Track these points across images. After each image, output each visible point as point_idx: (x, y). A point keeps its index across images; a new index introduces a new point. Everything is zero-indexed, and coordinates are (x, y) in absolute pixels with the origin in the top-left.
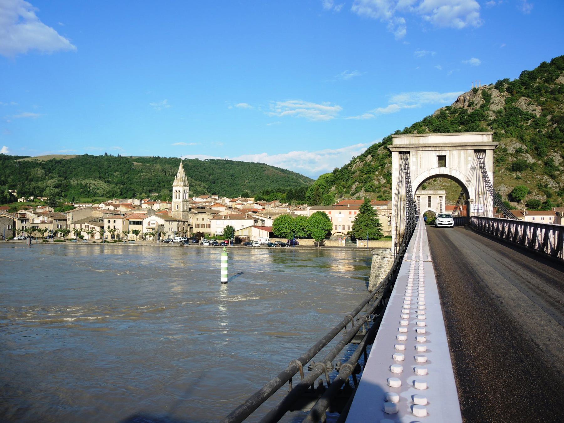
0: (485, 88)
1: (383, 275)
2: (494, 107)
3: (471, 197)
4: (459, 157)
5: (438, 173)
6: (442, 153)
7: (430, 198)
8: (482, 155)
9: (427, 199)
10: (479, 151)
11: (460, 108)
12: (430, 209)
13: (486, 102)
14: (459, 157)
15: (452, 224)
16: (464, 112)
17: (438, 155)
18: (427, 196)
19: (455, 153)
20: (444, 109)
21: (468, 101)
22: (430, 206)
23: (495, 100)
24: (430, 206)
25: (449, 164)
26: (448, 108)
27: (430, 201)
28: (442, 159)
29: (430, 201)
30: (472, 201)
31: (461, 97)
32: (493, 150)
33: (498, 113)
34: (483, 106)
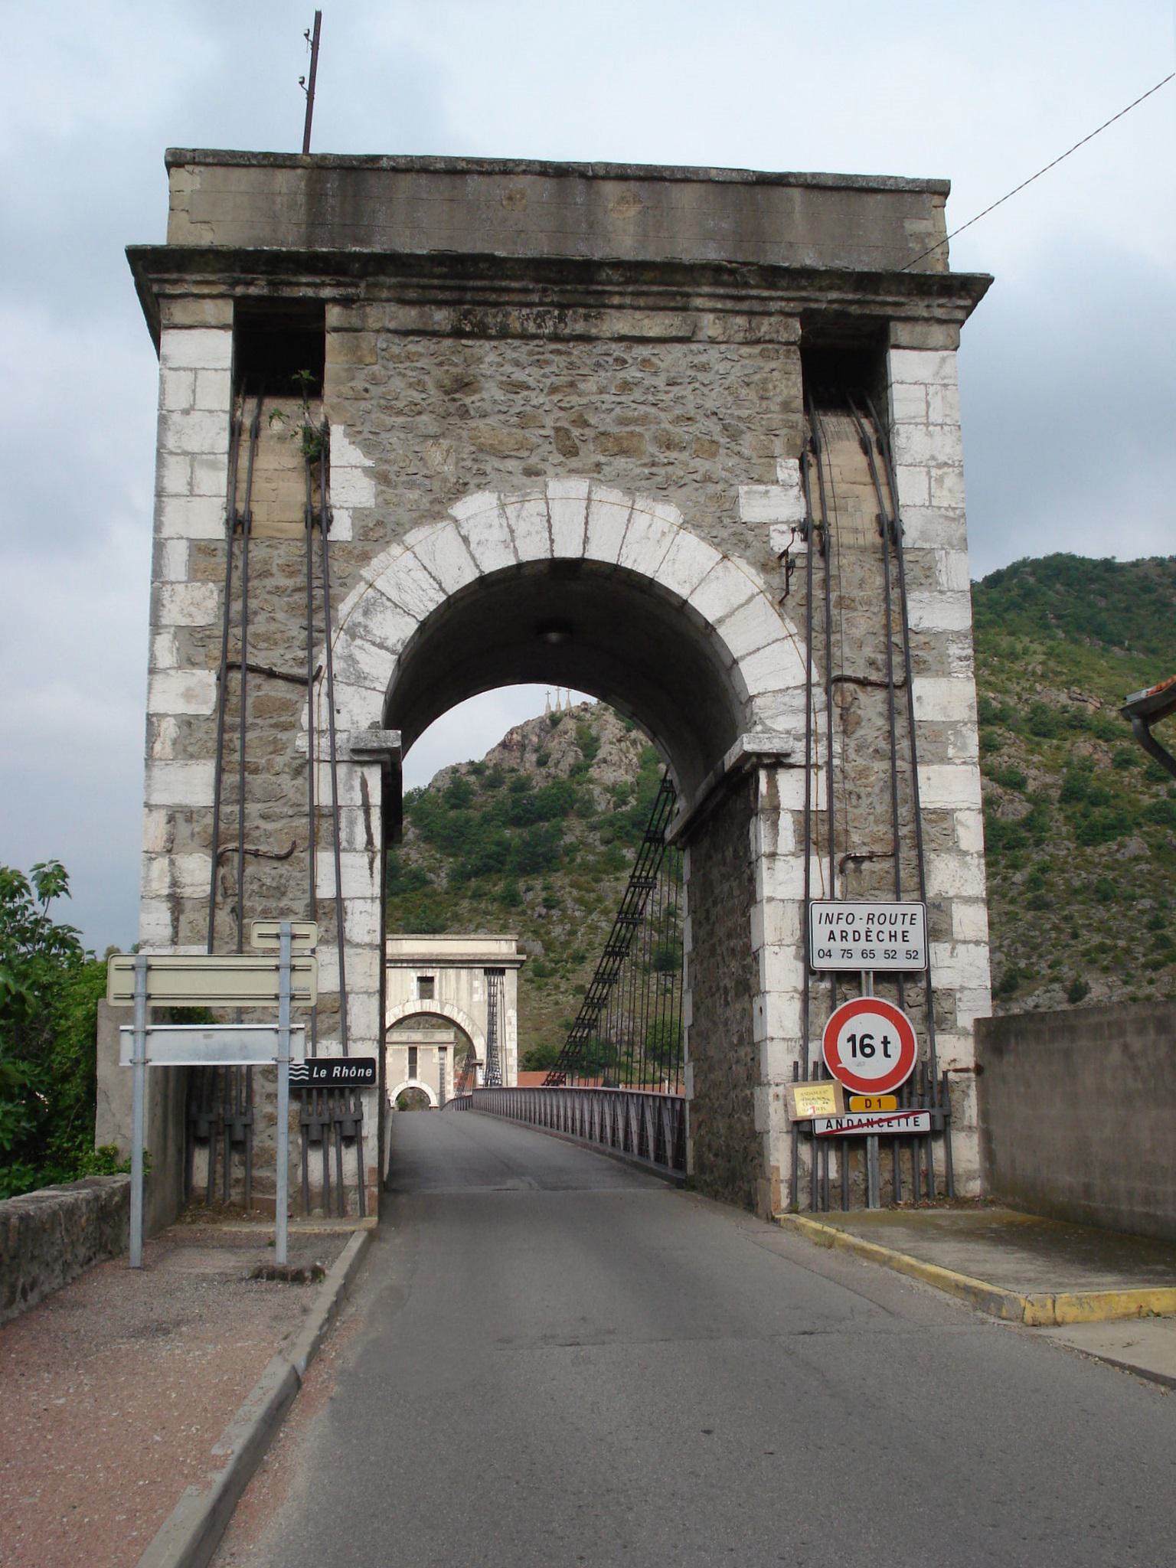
0: (585, 710)
1: (797, 304)
2: (609, 775)
3: (478, 1057)
4: (458, 977)
5: (419, 1010)
6: (429, 973)
7: (413, 1051)
8: (496, 979)
9: (407, 1055)
10: (494, 969)
11: (513, 770)
12: (413, 1083)
13: (585, 756)
14: (458, 977)
15: (261, 936)
16: (521, 786)
17: (419, 975)
18: (406, 1047)
19: (451, 972)
20: (464, 770)
21: (536, 751)
22: (413, 1073)
23: (611, 754)
24: (413, 1073)
25: (441, 994)
26: (476, 768)
27: (413, 1060)
28: (426, 982)
29: (413, 1060)
30: (481, 1065)
31: (515, 736)
32: (518, 969)
33: (619, 794)
34: (577, 770)
